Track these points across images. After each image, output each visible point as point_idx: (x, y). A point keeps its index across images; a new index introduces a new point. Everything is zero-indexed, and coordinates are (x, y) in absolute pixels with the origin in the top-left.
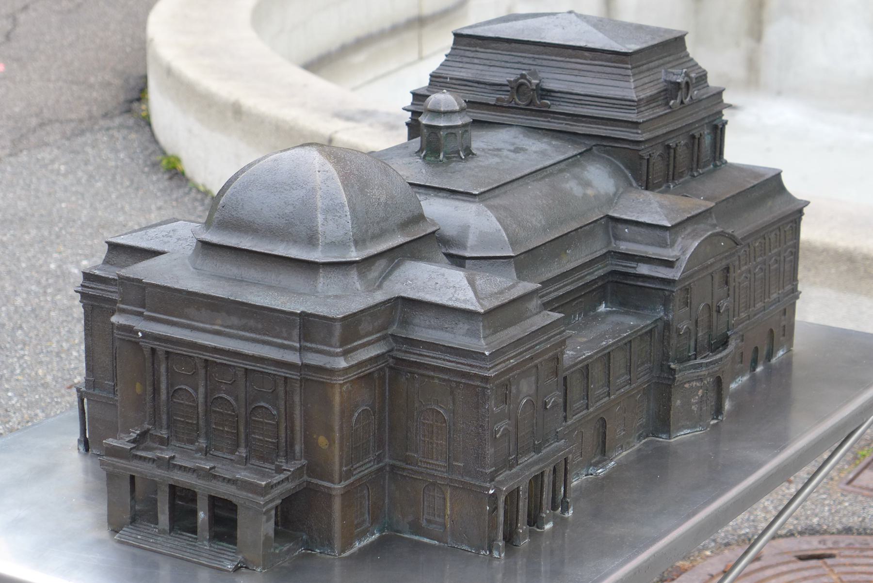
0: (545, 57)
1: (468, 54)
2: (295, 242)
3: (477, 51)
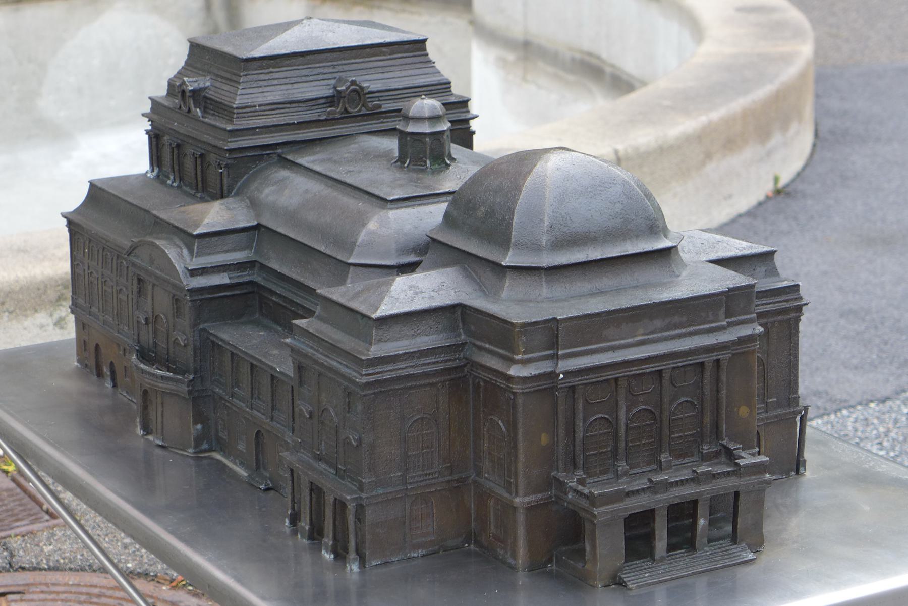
0: (344, 62)
1: (262, 77)
2: (637, 236)
3: (272, 72)
